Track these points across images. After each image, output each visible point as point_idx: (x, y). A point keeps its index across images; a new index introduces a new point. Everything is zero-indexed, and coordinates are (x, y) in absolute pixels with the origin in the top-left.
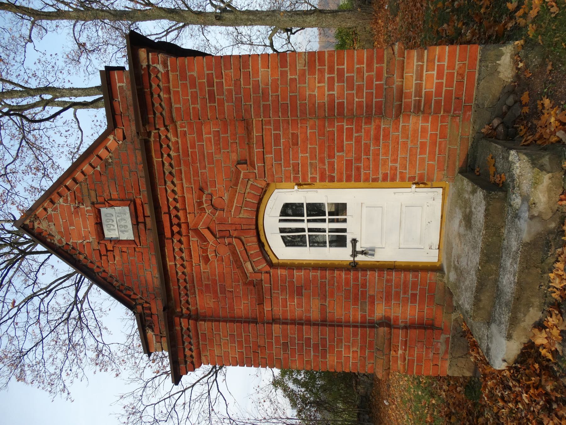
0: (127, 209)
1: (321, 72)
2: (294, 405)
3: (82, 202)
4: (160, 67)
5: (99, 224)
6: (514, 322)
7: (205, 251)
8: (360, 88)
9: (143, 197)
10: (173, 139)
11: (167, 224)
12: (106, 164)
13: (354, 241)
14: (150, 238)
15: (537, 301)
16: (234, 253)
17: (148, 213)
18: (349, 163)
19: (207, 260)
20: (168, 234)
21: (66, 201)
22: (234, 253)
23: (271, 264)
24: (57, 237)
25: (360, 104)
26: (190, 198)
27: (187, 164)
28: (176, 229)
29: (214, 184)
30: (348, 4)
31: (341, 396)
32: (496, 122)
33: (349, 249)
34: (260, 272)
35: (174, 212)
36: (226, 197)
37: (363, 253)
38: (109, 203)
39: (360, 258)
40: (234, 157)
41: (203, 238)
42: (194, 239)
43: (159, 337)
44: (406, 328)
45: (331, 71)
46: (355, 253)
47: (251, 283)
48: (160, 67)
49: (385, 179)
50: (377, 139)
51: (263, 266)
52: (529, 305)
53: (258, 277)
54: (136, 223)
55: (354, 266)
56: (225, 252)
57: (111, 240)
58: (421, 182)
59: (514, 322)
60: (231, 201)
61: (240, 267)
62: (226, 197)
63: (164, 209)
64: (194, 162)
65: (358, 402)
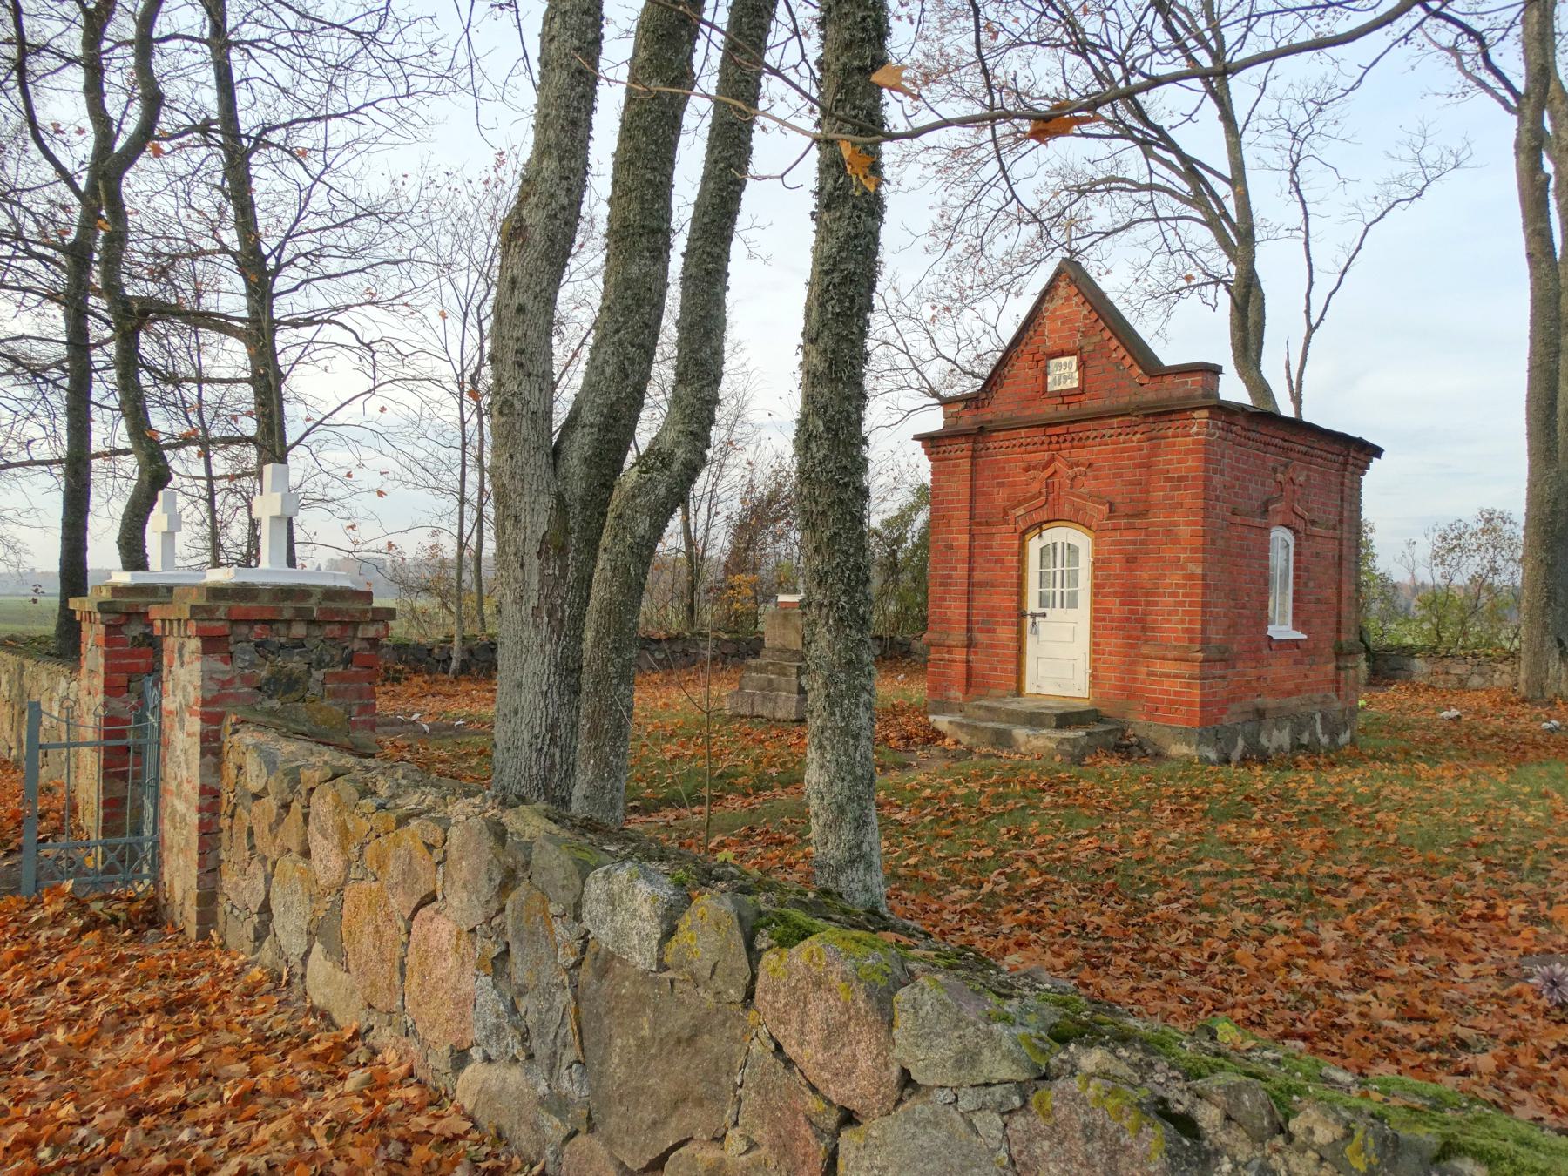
0: (1076, 385)
1: (1184, 586)
2: (888, 524)
3: (1084, 335)
4: (1195, 429)
5: (1063, 354)
6: (961, 726)
7: (1034, 468)
8: (1168, 621)
9: (1090, 405)
10: (1135, 438)
11: (1058, 430)
12: (1117, 365)
13: (1044, 615)
14: (1048, 410)
15: (974, 741)
16: (1033, 498)
17: (1072, 407)
18: (1109, 611)
19: (1027, 470)
20: (1050, 431)
21: (1085, 317)
22: (1033, 498)
23: (1024, 533)
24: (1051, 307)
25: (1155, 621)
26: (1082, 454)
27: (1113, 451)
28: (1054, 439)
29: (1096, 478)
30: (803, 536)
31: (907, 608)
32: (1133, 740)
33: (1037, 610)
34: (1016, 523)
35: (1069, 437)
36: (1084, 490)
37: (1034, 624)
38: (1082, 365)
39: (1029, 620)
40: (1118, 500)
41: (1045, 467)
42: (1047, 456)
43: (957, 416)
44: (968, 662)
45: (1186, 595)
46: (1034, 615)
47: (1006, 514)
48: (1195, 429)
49: (1096, 644)
50: (1129, 637)
51: (1022, 527)
52: (972, 736)
53: (1012, 521)
54: (1062, 394)
55: (1021, 615)
56: (1035, 487)
57: (1047, 366)
58: (1094, 678)
59: (961, 726)
60: (1079, 496)
61: (1020, 504)
62: (1084, 490)
63: (1072, 428)
64: (1116, 459)
65: (899, 638)
